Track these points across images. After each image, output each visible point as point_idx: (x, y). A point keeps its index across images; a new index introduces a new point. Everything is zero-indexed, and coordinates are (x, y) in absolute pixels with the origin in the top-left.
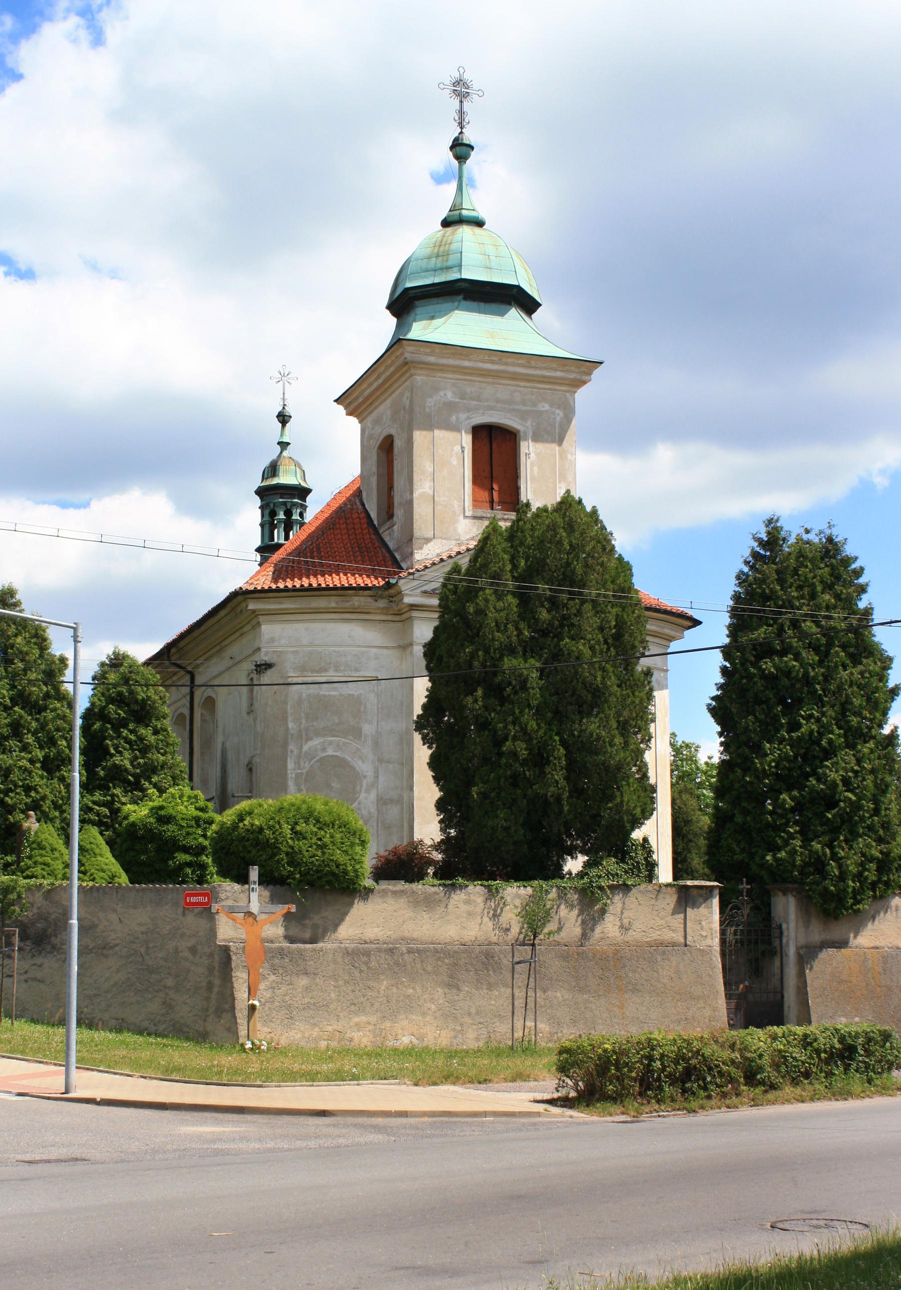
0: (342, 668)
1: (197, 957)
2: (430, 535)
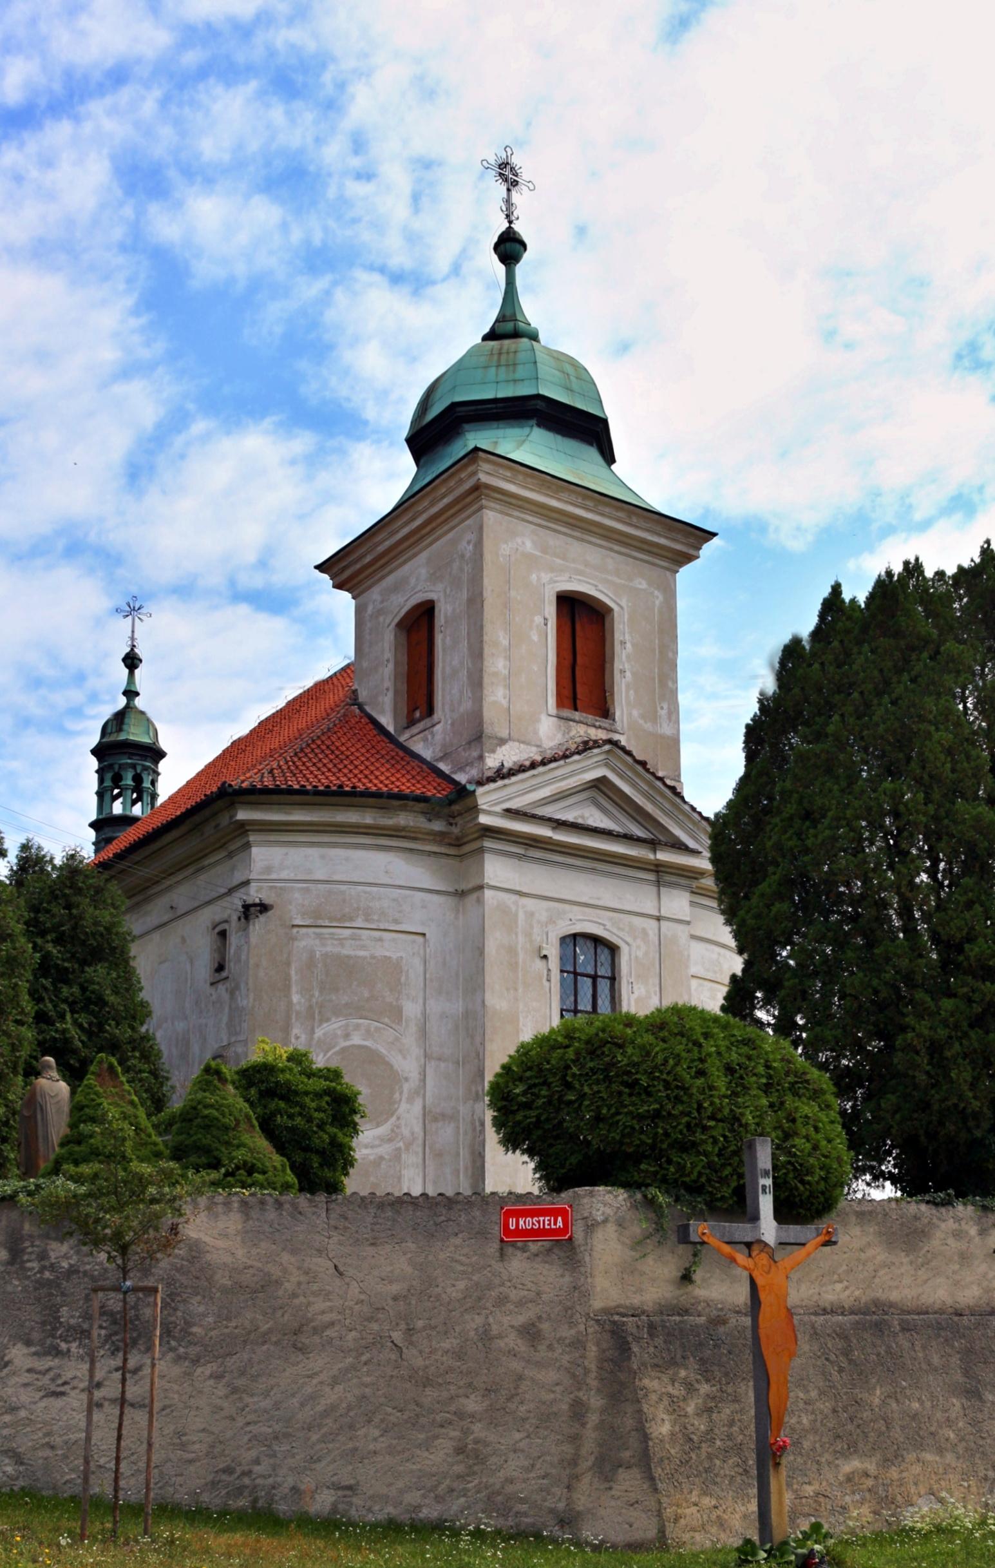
0: (376, 917)
1: (542, 1348)
2: (504, 734)
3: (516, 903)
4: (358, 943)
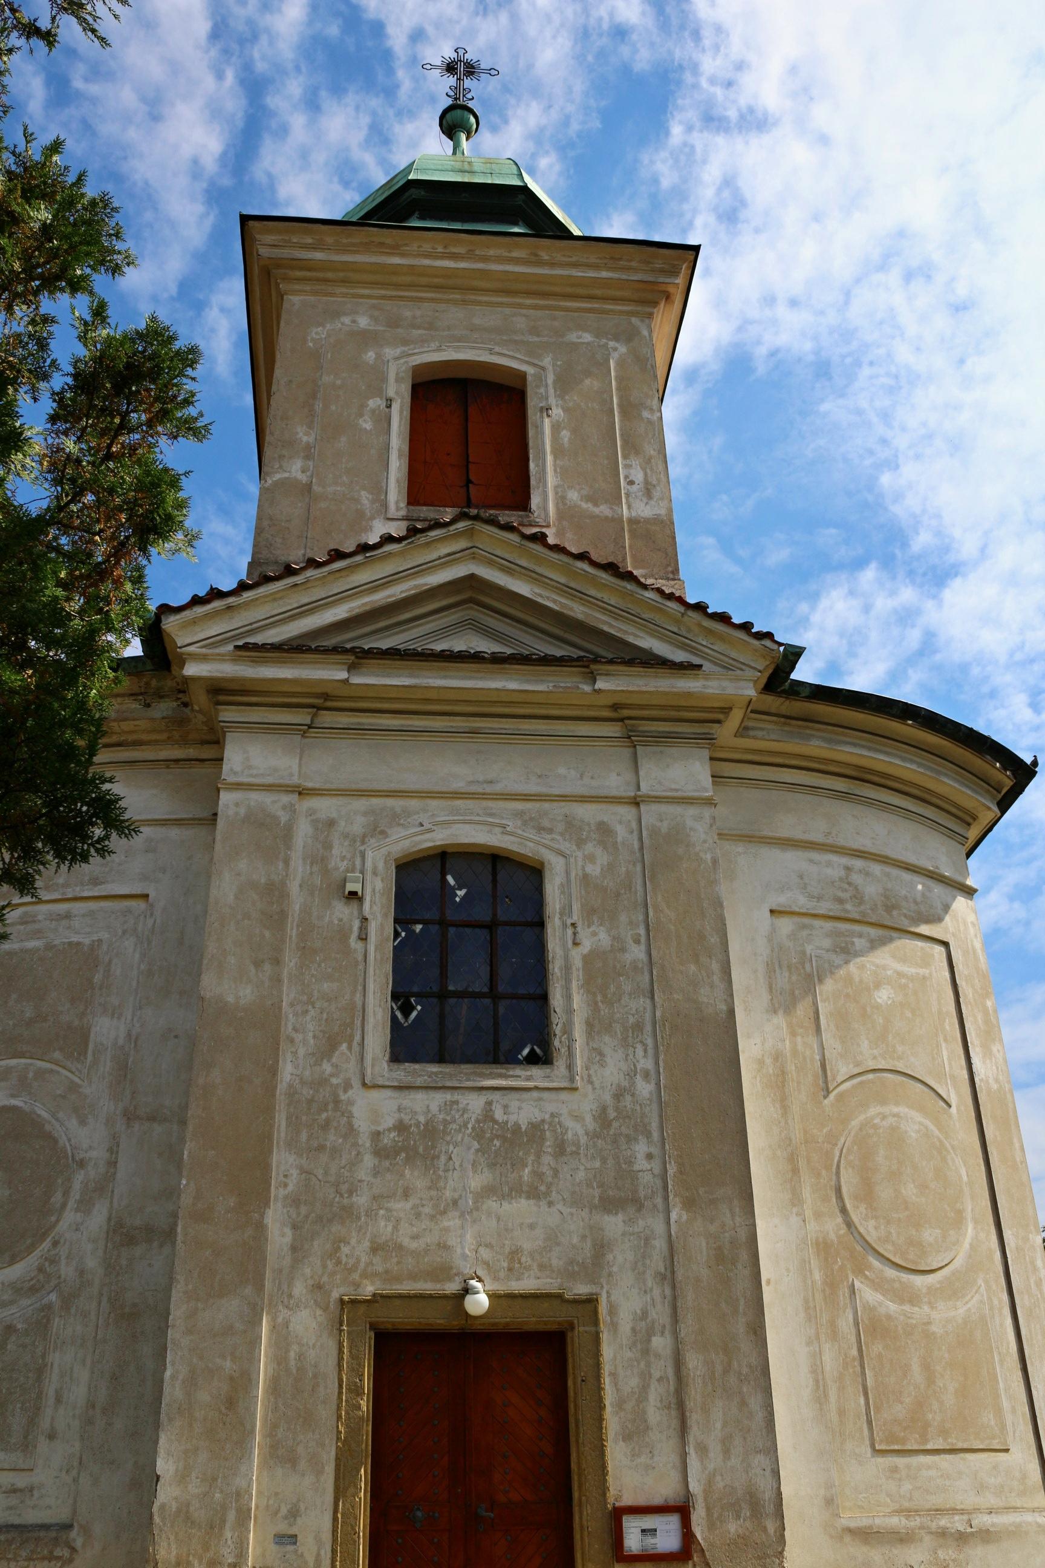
3: (291, 809)
4: (30, 927)
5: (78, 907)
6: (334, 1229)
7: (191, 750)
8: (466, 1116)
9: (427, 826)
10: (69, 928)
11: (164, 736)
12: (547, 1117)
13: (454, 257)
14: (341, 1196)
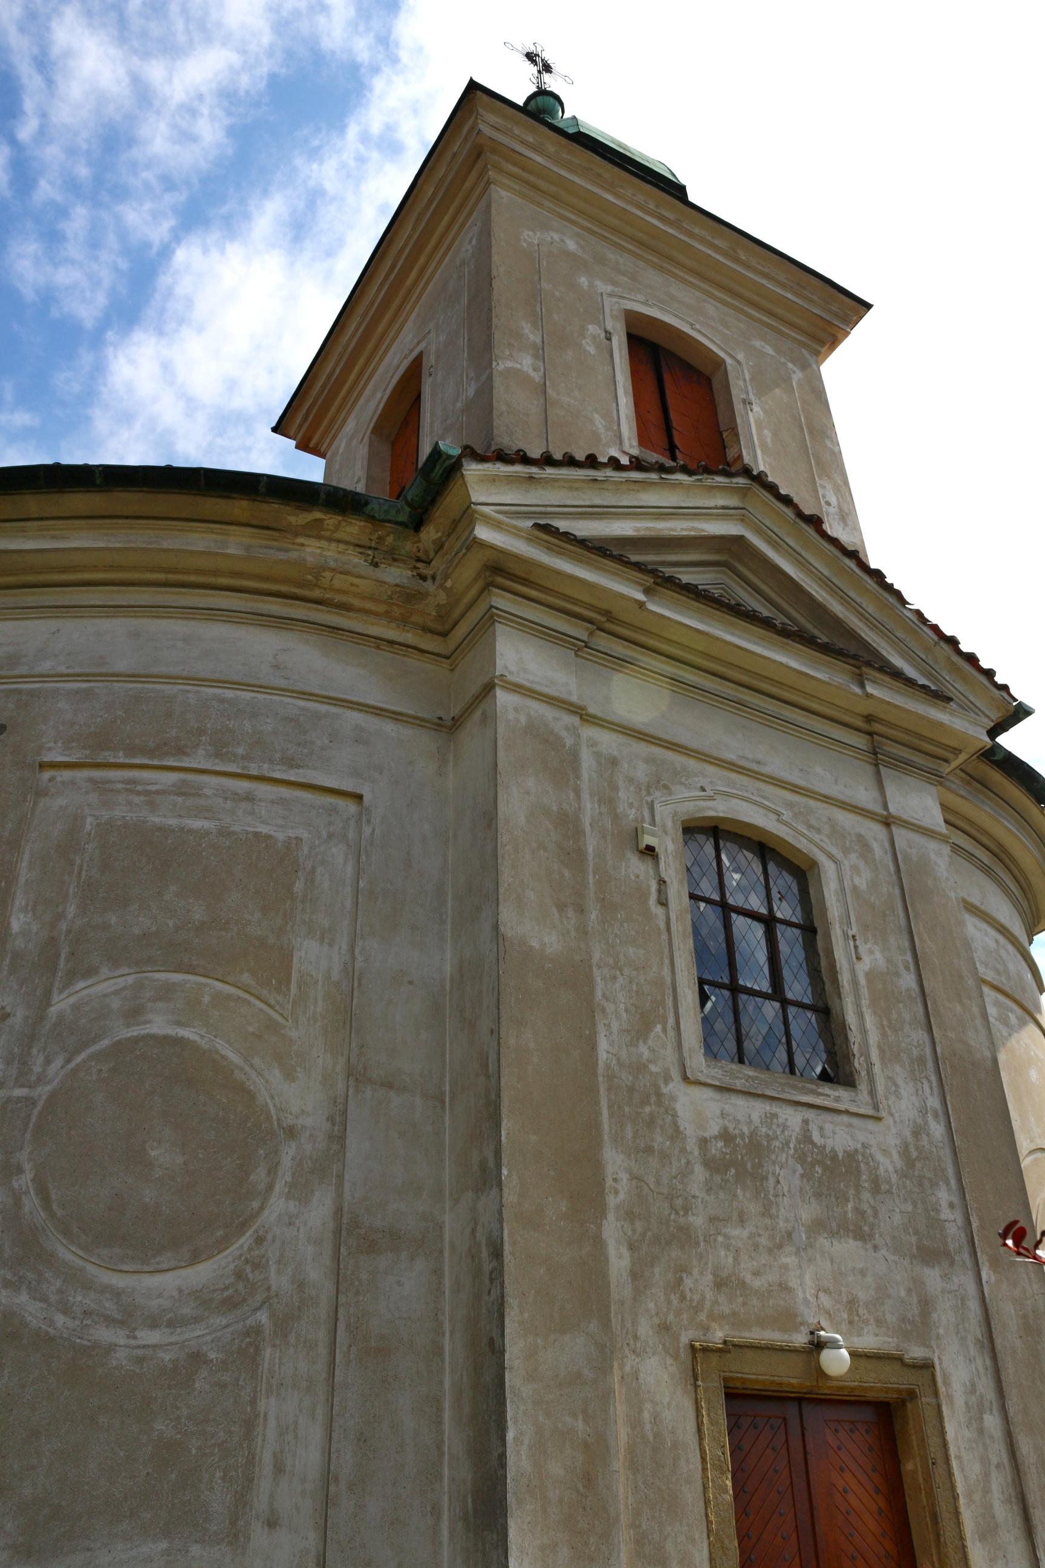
5: (263, 790)
6: (674, 1254)
7: (410, 635)
8: (786, 1133)
9: (709, 793)
10: (252, 813)
11: (381, 608)
12: (859, 1146)
13: (662, 218)
14: (677, 1213)
